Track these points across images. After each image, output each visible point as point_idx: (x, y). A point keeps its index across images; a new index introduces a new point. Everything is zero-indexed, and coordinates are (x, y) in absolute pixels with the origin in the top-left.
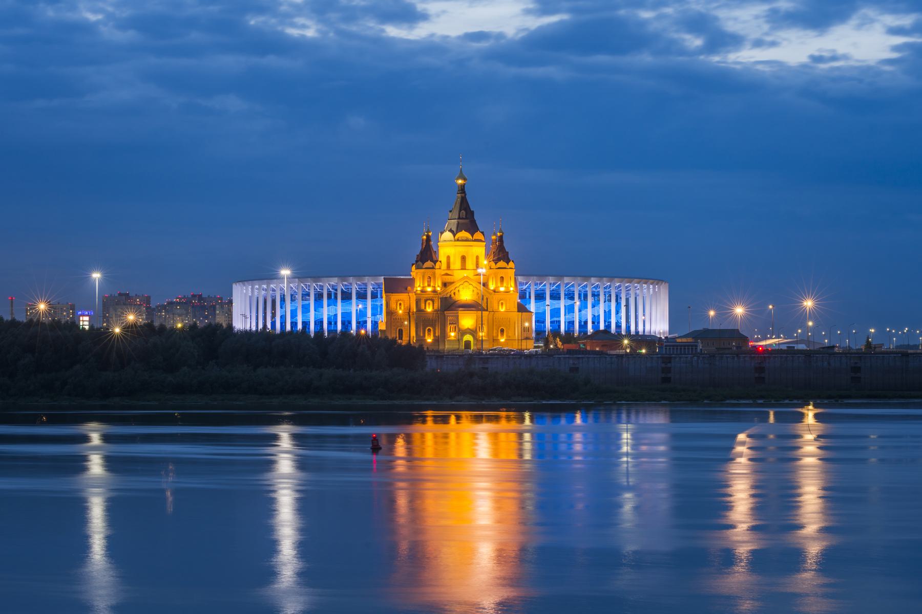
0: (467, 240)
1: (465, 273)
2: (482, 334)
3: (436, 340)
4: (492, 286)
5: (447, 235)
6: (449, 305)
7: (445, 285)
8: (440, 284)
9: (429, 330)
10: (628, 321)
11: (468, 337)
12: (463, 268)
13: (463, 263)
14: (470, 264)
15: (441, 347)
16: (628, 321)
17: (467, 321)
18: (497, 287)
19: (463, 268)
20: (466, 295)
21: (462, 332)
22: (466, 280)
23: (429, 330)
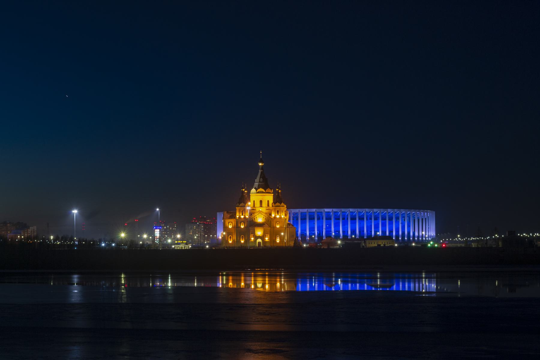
0: (263, 192)
1: (261, 209)
2: (267, 239)
4: (273, 215)
5: (253, 190)
6: (252, 224)
8: (248, 214)
9: (230, 237)
10: (397, 231)
11: (259, 240)
12: (261, 206)
13: (260, 203)
14: (265, 204)
15: (248, 245)
16: (397, 231)
17: (259, 232)
18: (275, 216)
19: (261, 206)
20: (260, 219)
21: (256, 238)
22: (260, 212)
23: (230, 237)
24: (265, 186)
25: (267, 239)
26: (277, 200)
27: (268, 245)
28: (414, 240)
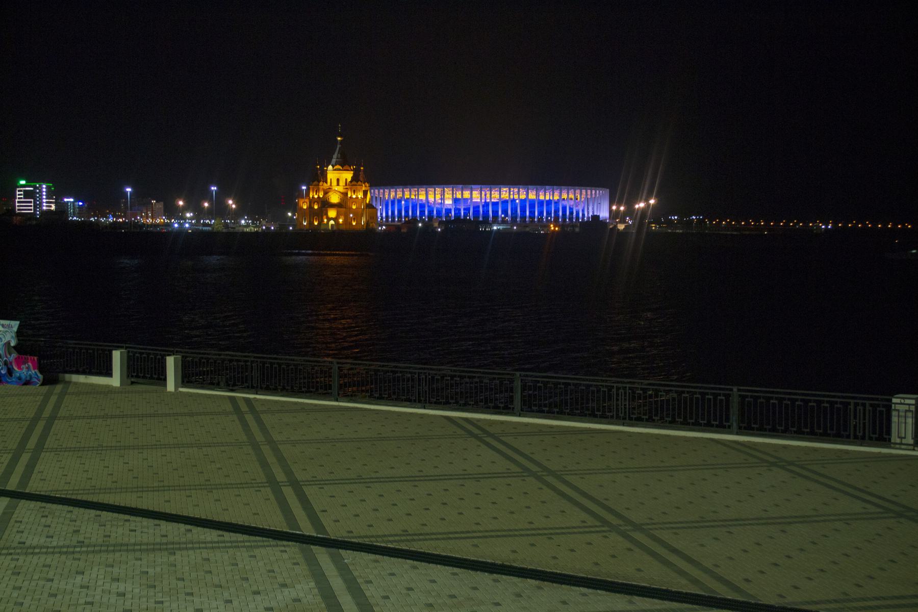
0: (340, 170)
1: (337, 188)
5: (330, 167)
6: (325, 204)
7: (326, 193)
12: (338, 185)
14: (342, 183)
17: (332, 213)
19: (338, 185)
20: (334, 199)
21: (329, 219)
24: (344, 164)
25: (341, 221)
26: (355, 179)
27: (341, 227)
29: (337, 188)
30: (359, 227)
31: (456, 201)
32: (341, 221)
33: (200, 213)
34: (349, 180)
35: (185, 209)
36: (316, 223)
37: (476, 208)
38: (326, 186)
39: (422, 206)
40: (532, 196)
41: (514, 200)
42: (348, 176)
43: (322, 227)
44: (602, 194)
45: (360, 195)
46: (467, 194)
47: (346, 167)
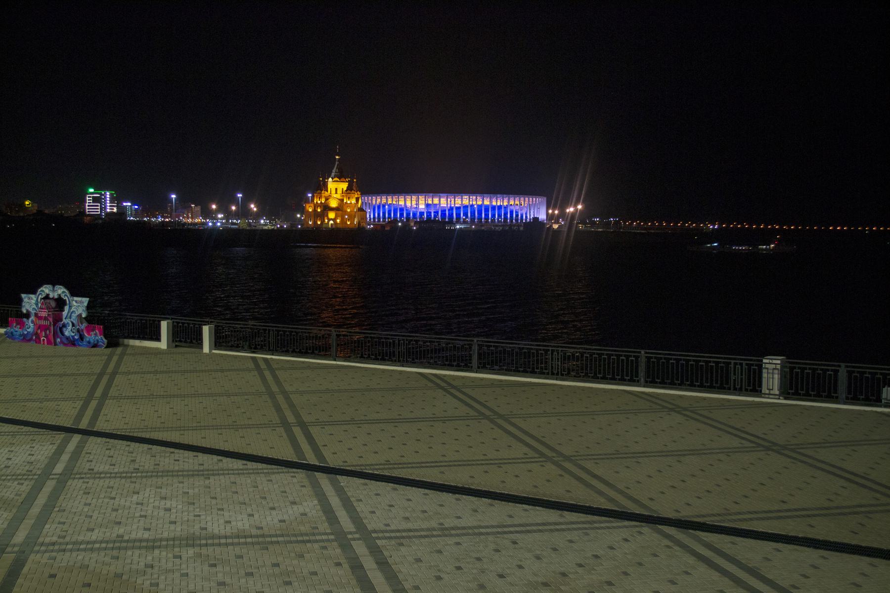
1: (335, 196)
3: (322, 223)
5: (330, 179)
6: (326, 208)
7: (327, 199)
14: (339, 191)
17: (332, 215)
20: (333, 204)
21: (329, 220)
24: (341, 177)
25: (338, 221)
26: (350, 188)
27: (339, 226)
28: (458, 221)
29: (335, 196)
30: (353, 226)
31: (428, 205)
32: (338, 221)
33: (229, 215)
34: (345, 189)
35: (218, 211)
36: (319, 223)
37: (443, 212)
38: (327, 194)
39: (402, 210)
40: (487, 202)
41: (472, 206)
42: (344, 186)
43: (324, 226)
44: (541, 201)
45: (354, 201)
46: (436, 201)
47: (343, 179)
